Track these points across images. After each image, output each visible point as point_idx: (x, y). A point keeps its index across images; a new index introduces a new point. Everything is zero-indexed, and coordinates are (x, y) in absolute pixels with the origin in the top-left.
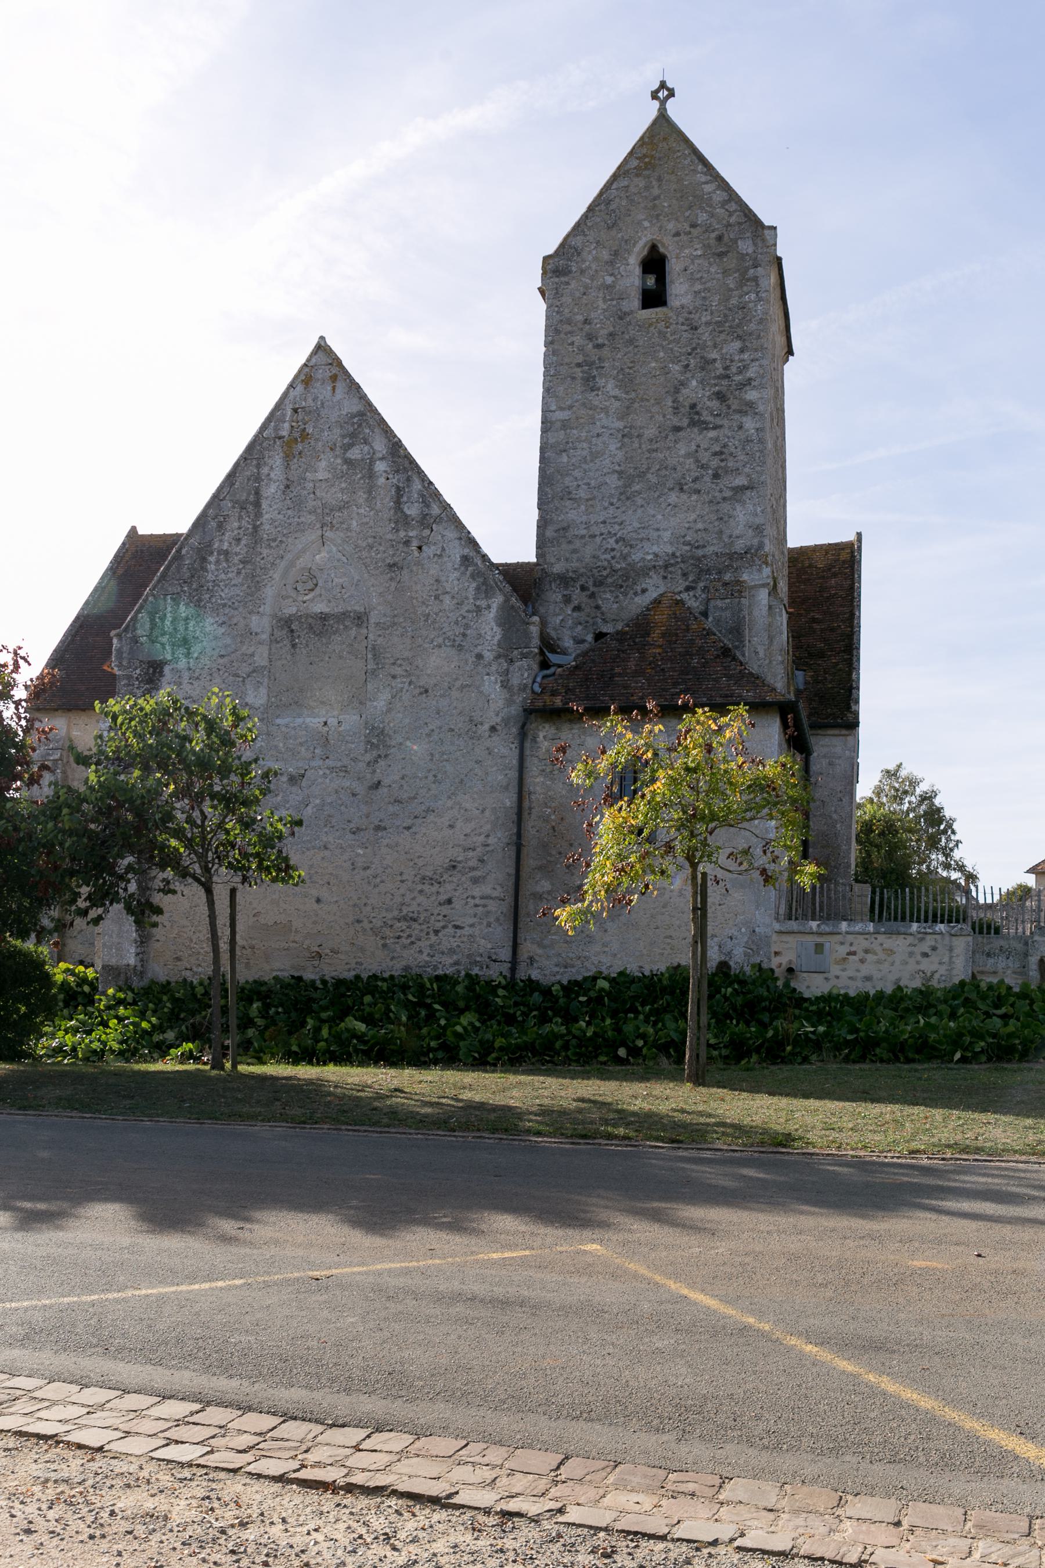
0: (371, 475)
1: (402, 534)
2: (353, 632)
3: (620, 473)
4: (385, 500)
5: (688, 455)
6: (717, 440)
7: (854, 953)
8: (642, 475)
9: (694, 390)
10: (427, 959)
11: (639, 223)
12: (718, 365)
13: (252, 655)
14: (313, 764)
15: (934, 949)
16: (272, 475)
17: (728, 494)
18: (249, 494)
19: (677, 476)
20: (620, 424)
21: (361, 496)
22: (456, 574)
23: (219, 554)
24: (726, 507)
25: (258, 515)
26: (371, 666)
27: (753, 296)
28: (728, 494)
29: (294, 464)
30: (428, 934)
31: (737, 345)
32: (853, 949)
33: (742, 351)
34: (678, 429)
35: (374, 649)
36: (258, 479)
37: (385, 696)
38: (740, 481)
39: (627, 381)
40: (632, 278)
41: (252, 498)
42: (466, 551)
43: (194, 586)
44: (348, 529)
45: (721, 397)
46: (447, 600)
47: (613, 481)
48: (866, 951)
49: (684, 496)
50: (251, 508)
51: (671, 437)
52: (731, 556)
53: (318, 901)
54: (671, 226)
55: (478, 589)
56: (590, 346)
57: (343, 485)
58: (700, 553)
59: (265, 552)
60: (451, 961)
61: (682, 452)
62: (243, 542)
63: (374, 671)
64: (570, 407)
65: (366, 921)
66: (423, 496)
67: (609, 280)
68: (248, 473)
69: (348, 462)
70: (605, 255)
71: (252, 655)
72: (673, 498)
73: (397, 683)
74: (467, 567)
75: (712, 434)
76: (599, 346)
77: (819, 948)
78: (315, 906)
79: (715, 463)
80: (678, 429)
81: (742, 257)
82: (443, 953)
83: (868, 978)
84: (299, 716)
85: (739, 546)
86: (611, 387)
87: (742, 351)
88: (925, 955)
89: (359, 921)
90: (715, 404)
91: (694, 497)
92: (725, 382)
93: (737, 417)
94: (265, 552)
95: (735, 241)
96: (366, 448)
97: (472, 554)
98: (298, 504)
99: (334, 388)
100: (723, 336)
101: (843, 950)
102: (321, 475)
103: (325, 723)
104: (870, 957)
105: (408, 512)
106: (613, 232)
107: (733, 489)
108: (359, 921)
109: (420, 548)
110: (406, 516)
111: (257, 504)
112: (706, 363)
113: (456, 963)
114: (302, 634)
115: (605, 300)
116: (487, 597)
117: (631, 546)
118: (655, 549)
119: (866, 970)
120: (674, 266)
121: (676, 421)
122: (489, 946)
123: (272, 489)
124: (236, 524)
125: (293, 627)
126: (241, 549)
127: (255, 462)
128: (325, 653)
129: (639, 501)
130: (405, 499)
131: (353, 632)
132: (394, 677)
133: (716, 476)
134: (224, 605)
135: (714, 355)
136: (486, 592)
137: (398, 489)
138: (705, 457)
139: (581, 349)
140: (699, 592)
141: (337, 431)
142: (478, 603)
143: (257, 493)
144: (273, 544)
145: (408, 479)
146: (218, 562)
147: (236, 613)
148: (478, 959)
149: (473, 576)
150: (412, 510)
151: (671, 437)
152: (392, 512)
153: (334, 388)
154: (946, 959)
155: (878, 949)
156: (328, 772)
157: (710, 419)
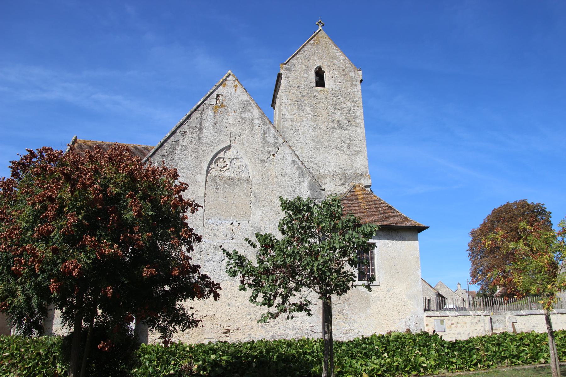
0: (252, 125)
1: (266, 148)
2: (245, 186)
3: (314, 140)
4: (259, 134)
5: (338, 138)
6: (348, 134)
7: (453, 324)
8: (321, 142)
9: (338, 115)
10: (282, 332)
11: (315, 60)
12: (346, 109)
13: (197, 191)
14: (226, 241)
15: (479, 321)
16: (208, 118)
17: (354, 153)
18: (197, 124)
19: (335, 144)
20: (312, 123)
21: (248, 132)
22: (290, 167)
23: (182, 147)
24: (353, 157)
25: (201, 133)
26: (253, 200)
27: (356, 90)
28: (354, 153)
29: (218, 115)
30: (282, 320)
31: (353, 104)
32: (453, 322)
33: (354, 106)
34: (334, 128)
35: (255, 194)
36: (201, 119)
37: (260, 213)
38: (358, 149)
39: (314, 108)
40: (312, 76)
41: (198, 126)
42: (294, 159)
43: (169, 159)
44: (243, 144)
45: (349, 121)
46: (286, 177)
47: (311, 142)
48: (457, 323)
49: (338, 152)
50: (197, 129)
51: (331, 130)
52: (357, 174)
53: (229, 305)
54: (326, 63)
55: (299, 174)
56: (300, 95)
57: (240, 127)
58: (345, 172)
59: (204, 149)
60: (294, 333)
61: (336, 136)
62: (194, 143)
63: (254, 203)
64: (293, 115)
65: (253, 315)
66: (275, 135)
67: (306, 75)
68: (197, 116)
69: (242, 118)
70: (304, 67)
71: (197, 191)
72: (334, 151)
73: (265, 209)
74: (294, 165)
75: (346, 132)
76: (304, 96)
77: (442, 322)
78: (228, 307)
79: (348, 141)
80: (334, 128)
81: (351, 77)
82: (290, 329)
83: (459, 333)
84: (220, 220)
85: (359, 171)
86: (308, 110)
87: (354, 106)
88: (476, 323)
89: (249, 315)
90: (346, 122)
91: (342, 152)
92: (349, 115)
93: (354, 127)
94: (204, 149)
95: (349, 72)
96: (250, 114)
97: (297, 160)
98: (220, 131)
99: (236, 90)
100: (347, 101)
101: (450, 322)
102: (231, 121)
103: (232, 223)
104: (458, 325)
105: (269, 141)
106: (306, 61)
107: (355, 151)
108: (249, 315)
109: (274, 155)
110: (268, 142)
111: (201, 129)
112: (342, 109)
113: (296, 334)
114: (221, 184)
115: (305, 82)
116: (303, 177)
117: (319, 167)
118: (329, 169)
119: (458, 330)
120: (326, 76)
121: (333, 126)
122: (311, 325)
123: (208, 124)
124: (190, 136)
125: (217, 181)
126: (193, 146)
127: (200, 112)
128: (232, 193)
129: (321, 151)
130: (267, 135)
131: (245, 186)
132: (264, 206)
133: (349, 146)
134: (184, 168)
135: (344, 106)
136: (303, 175)
137: (264, 131)
138: (344, 139)
139: (297, 96)
140: (346, 186)
141: (237, 105)
142: (300, 179)
143: (201, 124)
144: (208, 146)
145: (269, 128)
146: (181, 150)
147: (189, 172)
148: (306, 331)
149: (297, 168)
150: (271, 140)
151: (331, 130)
152: (262, 140)
153: (236, 90)
154: (483, 325)
155: (461, 321)
156: (233, 245)
157: (344, 126)
